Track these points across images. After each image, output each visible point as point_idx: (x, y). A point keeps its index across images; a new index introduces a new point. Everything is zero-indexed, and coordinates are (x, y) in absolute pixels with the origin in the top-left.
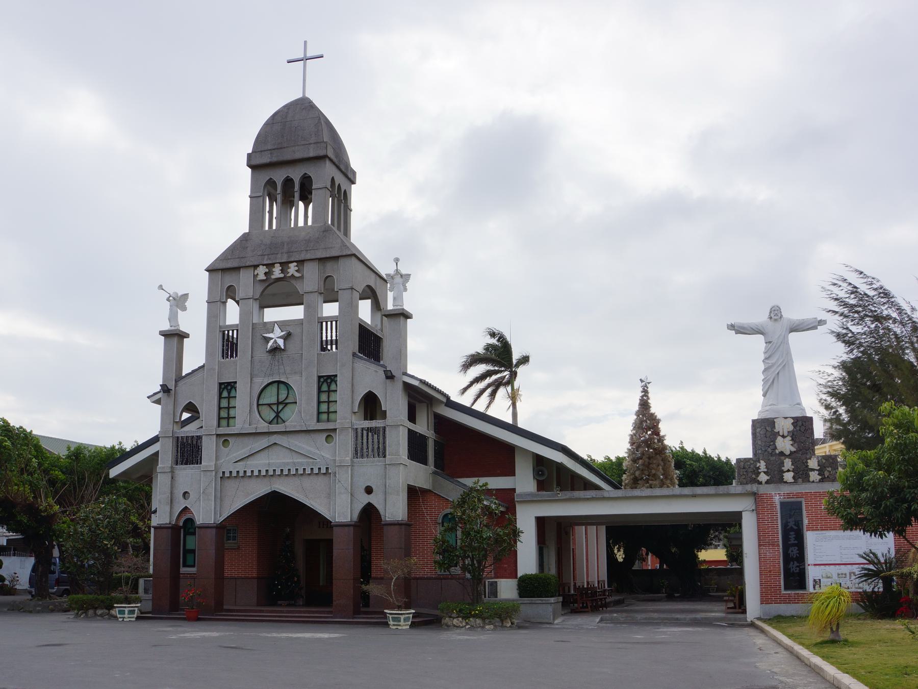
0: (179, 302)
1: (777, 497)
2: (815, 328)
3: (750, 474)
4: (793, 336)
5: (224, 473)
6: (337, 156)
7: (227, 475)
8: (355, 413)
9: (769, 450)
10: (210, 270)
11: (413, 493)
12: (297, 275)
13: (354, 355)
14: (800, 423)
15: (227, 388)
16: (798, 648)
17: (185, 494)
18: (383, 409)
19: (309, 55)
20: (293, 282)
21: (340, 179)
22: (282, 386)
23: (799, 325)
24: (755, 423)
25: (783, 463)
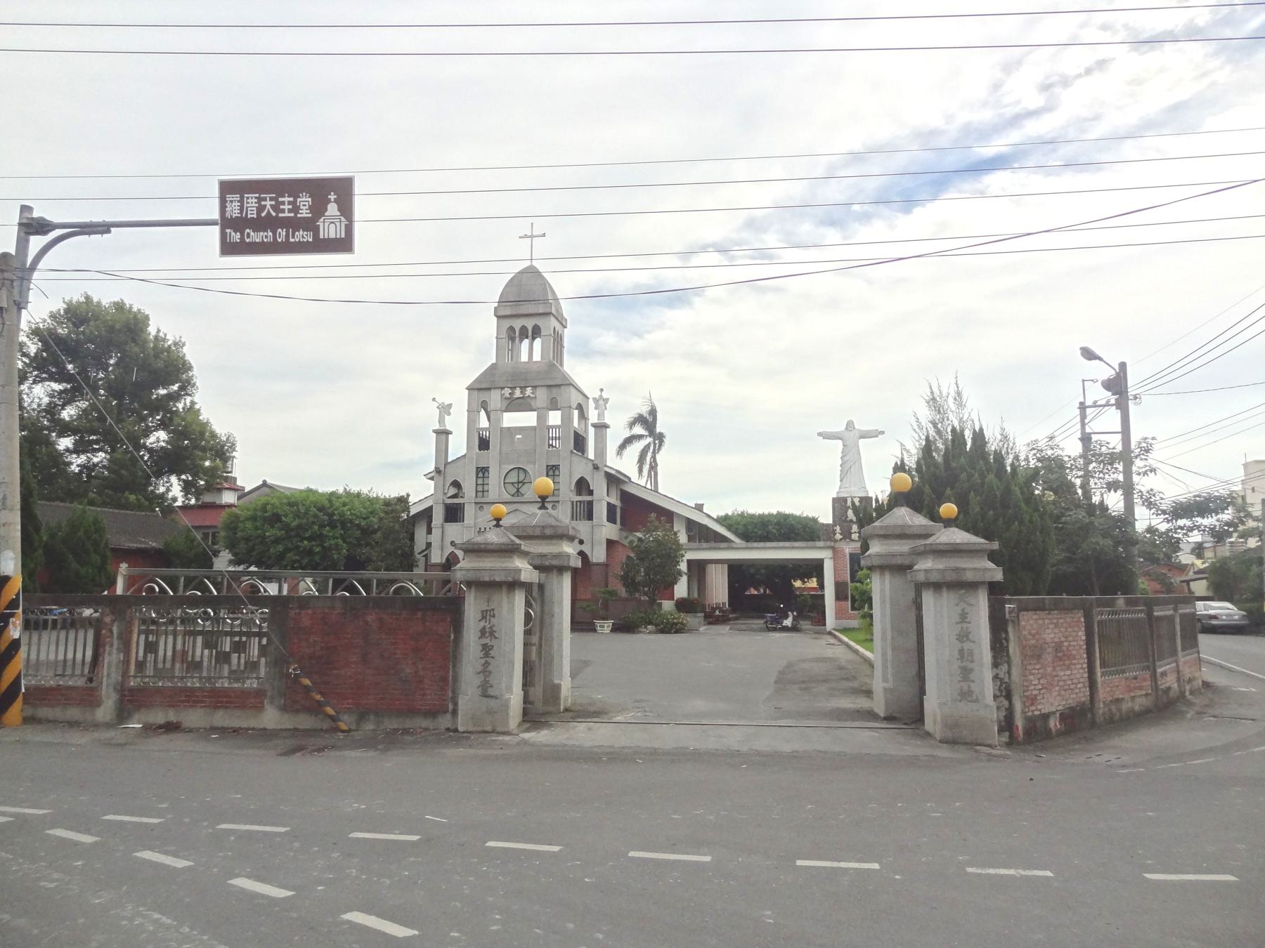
0: (445, 409)
2: (877, 436)
4: (861, 441)
5: (480, 529)
6: (557, 311)
7: (483, 530)
8: (571, 491)
11: (610, 544)
12: (531, 395)
13: (572, 452)
14: (864, 501)
15: (482, 471)
16: (852, 643)
18: (591, 488)
21: (558, 327)
22: (521, 471)
24: (835, 500)
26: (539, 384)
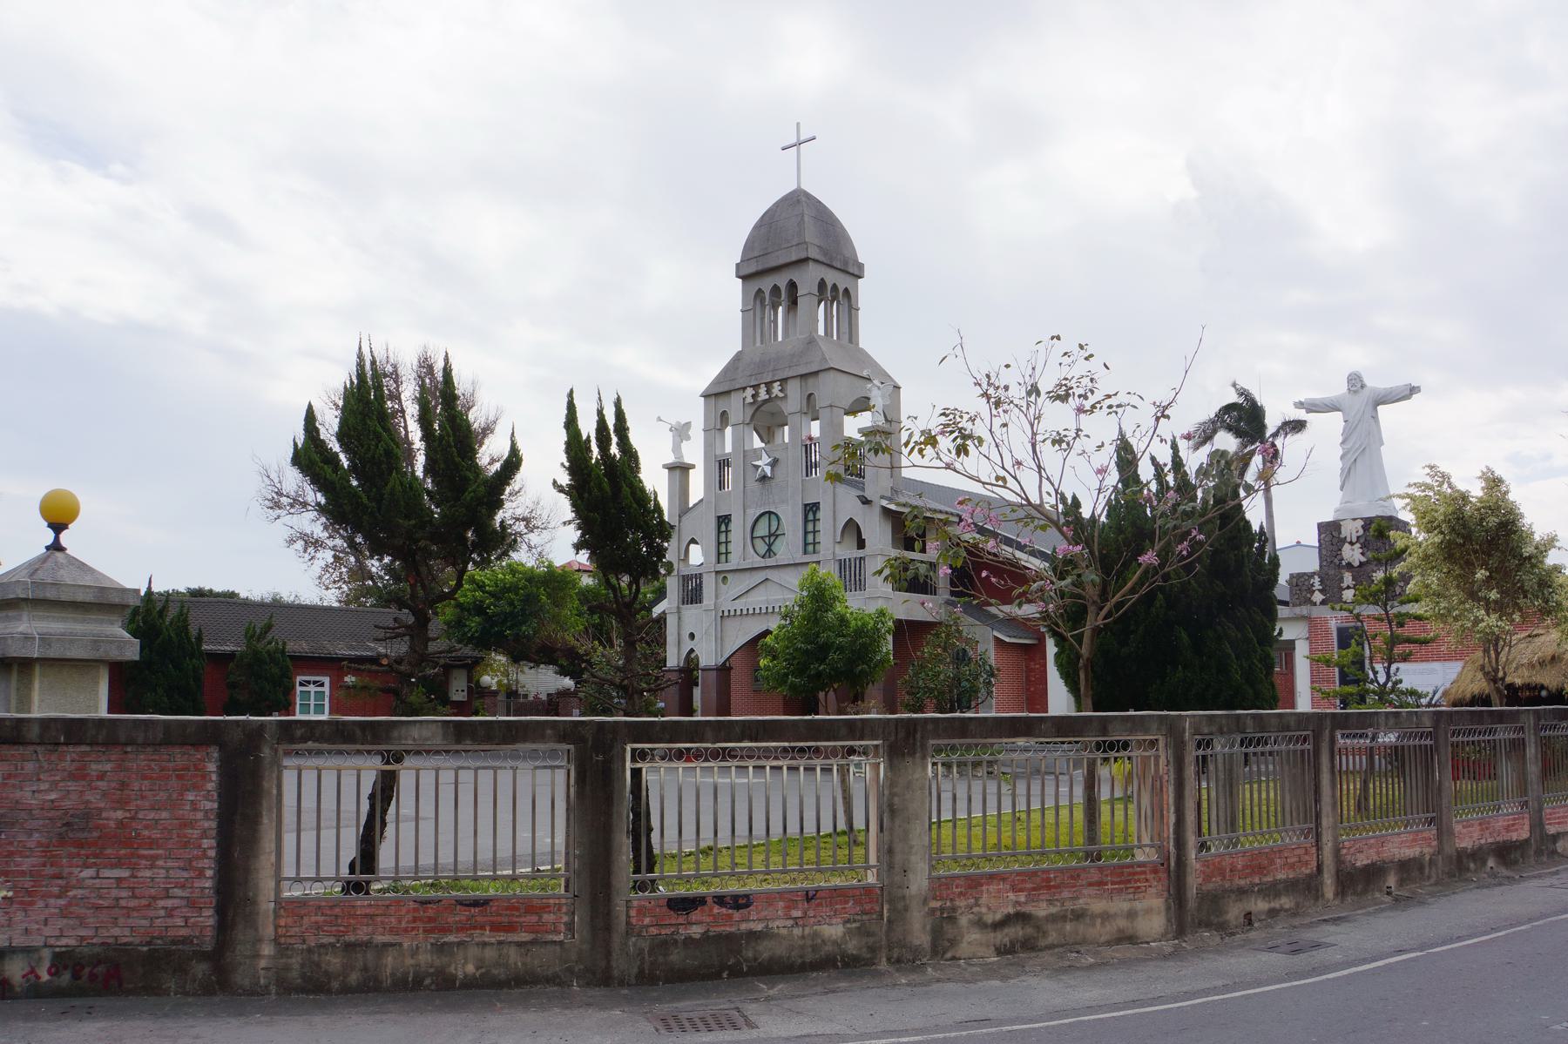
1: (1334, 622)
2: (1407, 397)
3: (1304, 593)
7: (726, 614)
9: (1336, 561)
10: (706, 396)
12: (781, 395)
15: (724, 521)
17: (692, 636)
19: (802, 139)
20: (779, 403)
23: (1383, 397)
25: (1342, 578)
26: (791, 374)
